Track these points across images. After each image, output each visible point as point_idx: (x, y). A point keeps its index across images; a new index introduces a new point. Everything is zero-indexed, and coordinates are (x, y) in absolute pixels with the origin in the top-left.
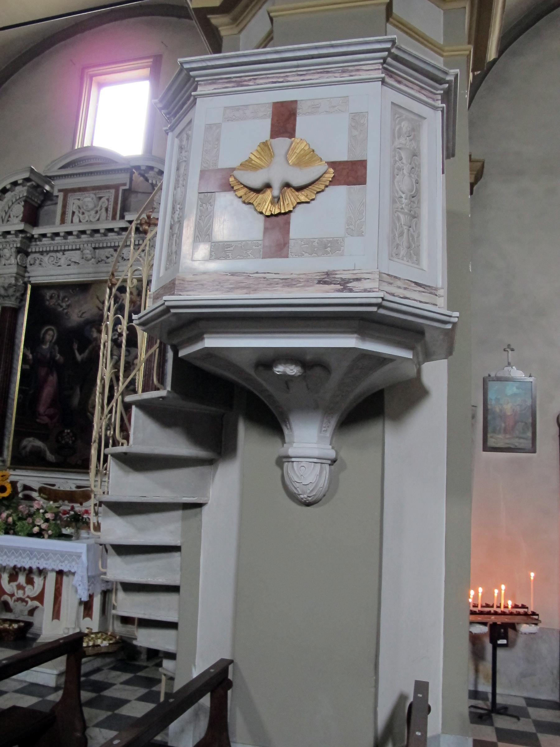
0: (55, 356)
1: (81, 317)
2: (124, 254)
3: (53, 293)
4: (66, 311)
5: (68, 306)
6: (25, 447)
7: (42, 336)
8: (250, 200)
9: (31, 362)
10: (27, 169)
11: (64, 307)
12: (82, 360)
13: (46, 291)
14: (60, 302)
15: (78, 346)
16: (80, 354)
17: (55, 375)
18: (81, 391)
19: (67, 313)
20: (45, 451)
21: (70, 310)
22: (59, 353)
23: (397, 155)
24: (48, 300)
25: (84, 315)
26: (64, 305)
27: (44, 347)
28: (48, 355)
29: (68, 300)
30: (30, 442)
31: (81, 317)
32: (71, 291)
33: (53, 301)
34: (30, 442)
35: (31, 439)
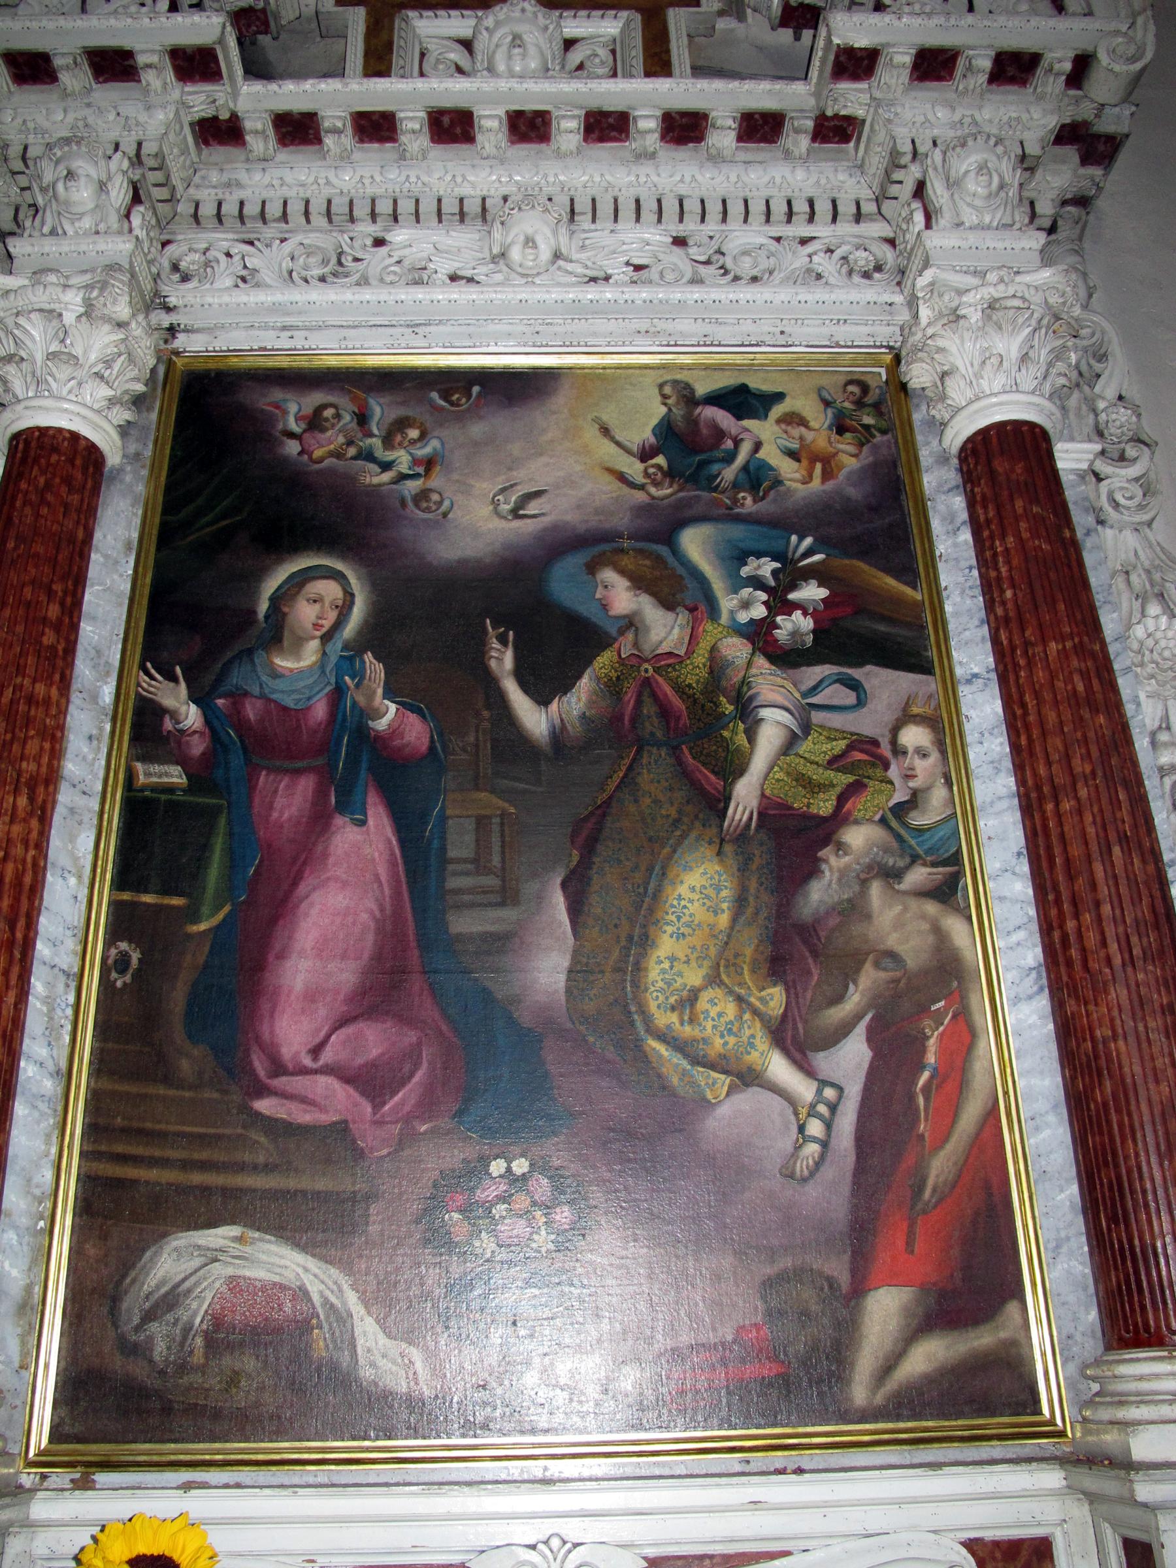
0: (368, 713)
1: (516, 513)
2: (76, 825)
3: (324, 407)
4: (413, 486)
5: (429, 464)
6: (171, 1300)
7: (263, 607)
8: (491, 249)
9: (197, 747)
10: (576, 112)
11: (404, 468)
12: (558, 736)
13: (277, 394)
14: (376, 442)
15: (518, 659)
16: (543, 701)
17: (378, 818)
18: (576, 910)
19: (422, 496)
20: (342, 1318)
21: (436, 481)
22: (390, 693)
23: (392, 268)
24: (291, 435)
25: (532, 508)
26: (403, 459)
27: (283, 663)
28: (320, 711)
29: (423, 436)
30: (213, 1257)
31: (516, 513)
32: (435, 395)
33: (332, 439)
34: (213, 1257)
35: (220, 1236)
